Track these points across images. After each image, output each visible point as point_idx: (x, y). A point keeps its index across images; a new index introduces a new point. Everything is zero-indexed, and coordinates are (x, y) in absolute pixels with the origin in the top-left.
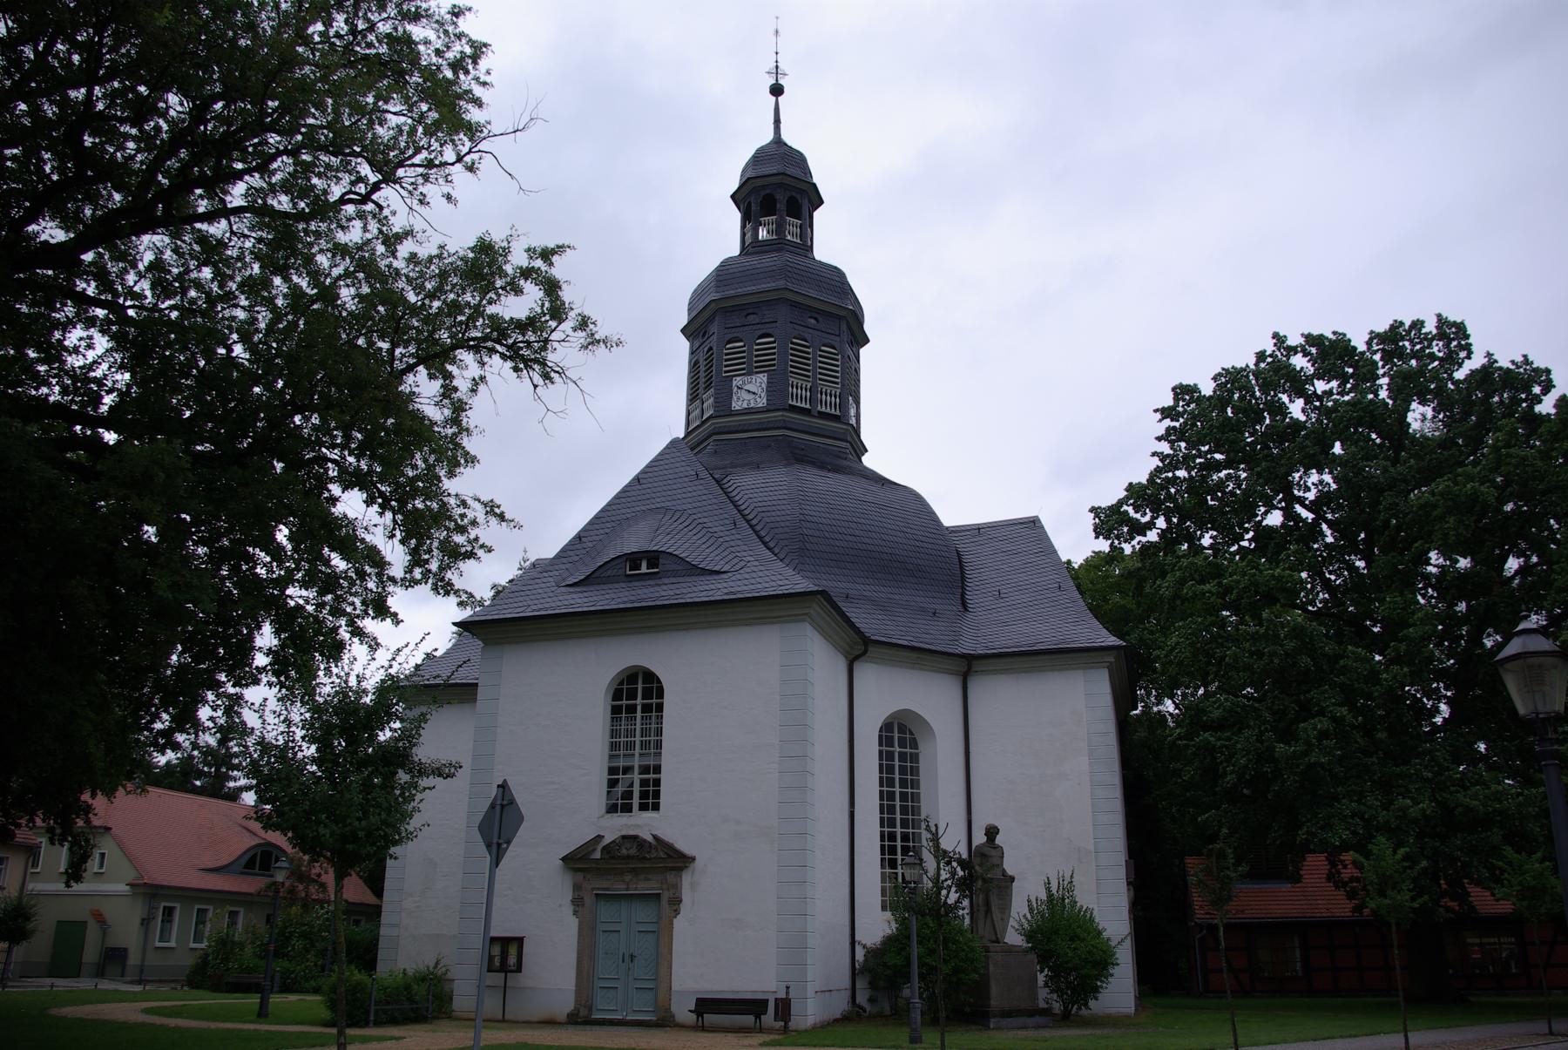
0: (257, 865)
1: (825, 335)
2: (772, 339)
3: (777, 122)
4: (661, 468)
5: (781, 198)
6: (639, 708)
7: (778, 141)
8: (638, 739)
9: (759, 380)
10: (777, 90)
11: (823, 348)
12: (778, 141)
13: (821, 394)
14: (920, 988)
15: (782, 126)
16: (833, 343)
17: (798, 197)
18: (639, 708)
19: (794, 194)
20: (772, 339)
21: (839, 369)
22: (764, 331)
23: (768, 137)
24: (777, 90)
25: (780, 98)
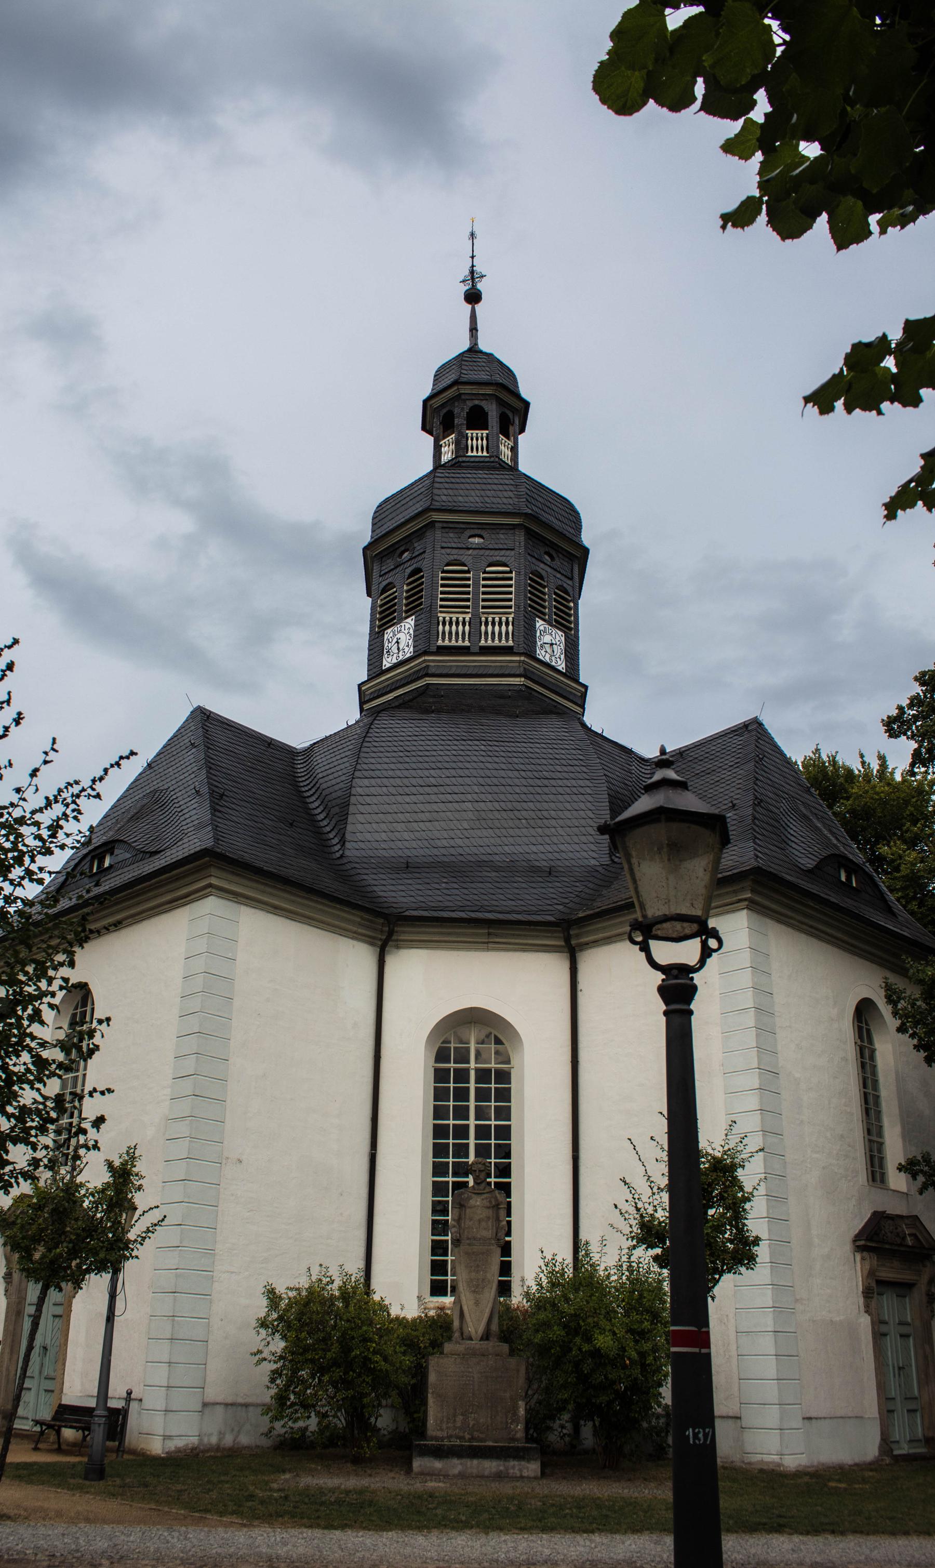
0: (506, 1279)
1: (492, 553)
2: (508, 569)
3: (474, 329)
4: (433, 759)
5: (493, 412)
6: (472, 1074)
7: (473, 350)
8: (472, 1122)
9: (407, 626)
10: (473, 297)
11: (488, 569)
12: (473, 350)
13: (444, 624)
14: (898, 900)
15: (480, 334)
16: (503, 559)
17: (510, 415)
18: (472, 1074)
19: (477, 402)
20: (508, 569)
21: (482, 589)
22: (495, 559)
23: (466, 345)
24: (473, 297)
25: (477, 307)
